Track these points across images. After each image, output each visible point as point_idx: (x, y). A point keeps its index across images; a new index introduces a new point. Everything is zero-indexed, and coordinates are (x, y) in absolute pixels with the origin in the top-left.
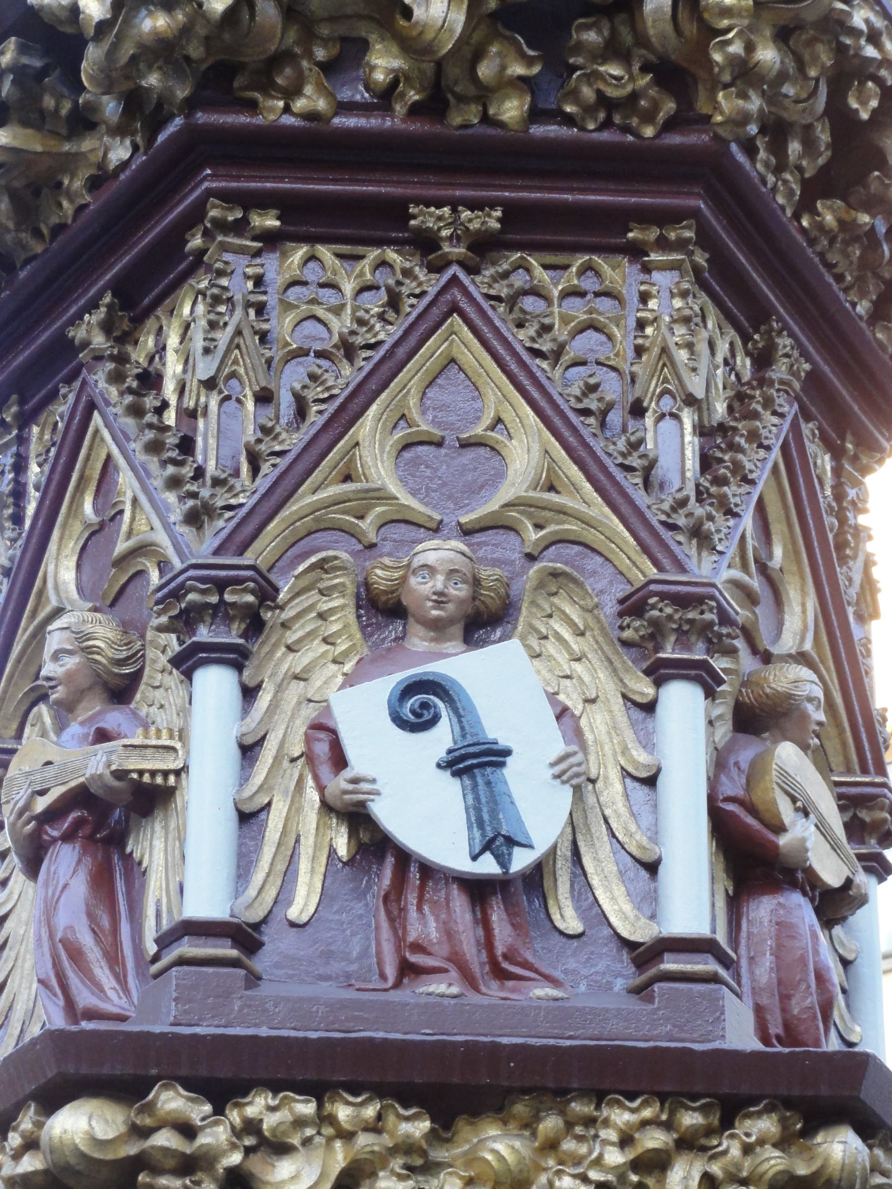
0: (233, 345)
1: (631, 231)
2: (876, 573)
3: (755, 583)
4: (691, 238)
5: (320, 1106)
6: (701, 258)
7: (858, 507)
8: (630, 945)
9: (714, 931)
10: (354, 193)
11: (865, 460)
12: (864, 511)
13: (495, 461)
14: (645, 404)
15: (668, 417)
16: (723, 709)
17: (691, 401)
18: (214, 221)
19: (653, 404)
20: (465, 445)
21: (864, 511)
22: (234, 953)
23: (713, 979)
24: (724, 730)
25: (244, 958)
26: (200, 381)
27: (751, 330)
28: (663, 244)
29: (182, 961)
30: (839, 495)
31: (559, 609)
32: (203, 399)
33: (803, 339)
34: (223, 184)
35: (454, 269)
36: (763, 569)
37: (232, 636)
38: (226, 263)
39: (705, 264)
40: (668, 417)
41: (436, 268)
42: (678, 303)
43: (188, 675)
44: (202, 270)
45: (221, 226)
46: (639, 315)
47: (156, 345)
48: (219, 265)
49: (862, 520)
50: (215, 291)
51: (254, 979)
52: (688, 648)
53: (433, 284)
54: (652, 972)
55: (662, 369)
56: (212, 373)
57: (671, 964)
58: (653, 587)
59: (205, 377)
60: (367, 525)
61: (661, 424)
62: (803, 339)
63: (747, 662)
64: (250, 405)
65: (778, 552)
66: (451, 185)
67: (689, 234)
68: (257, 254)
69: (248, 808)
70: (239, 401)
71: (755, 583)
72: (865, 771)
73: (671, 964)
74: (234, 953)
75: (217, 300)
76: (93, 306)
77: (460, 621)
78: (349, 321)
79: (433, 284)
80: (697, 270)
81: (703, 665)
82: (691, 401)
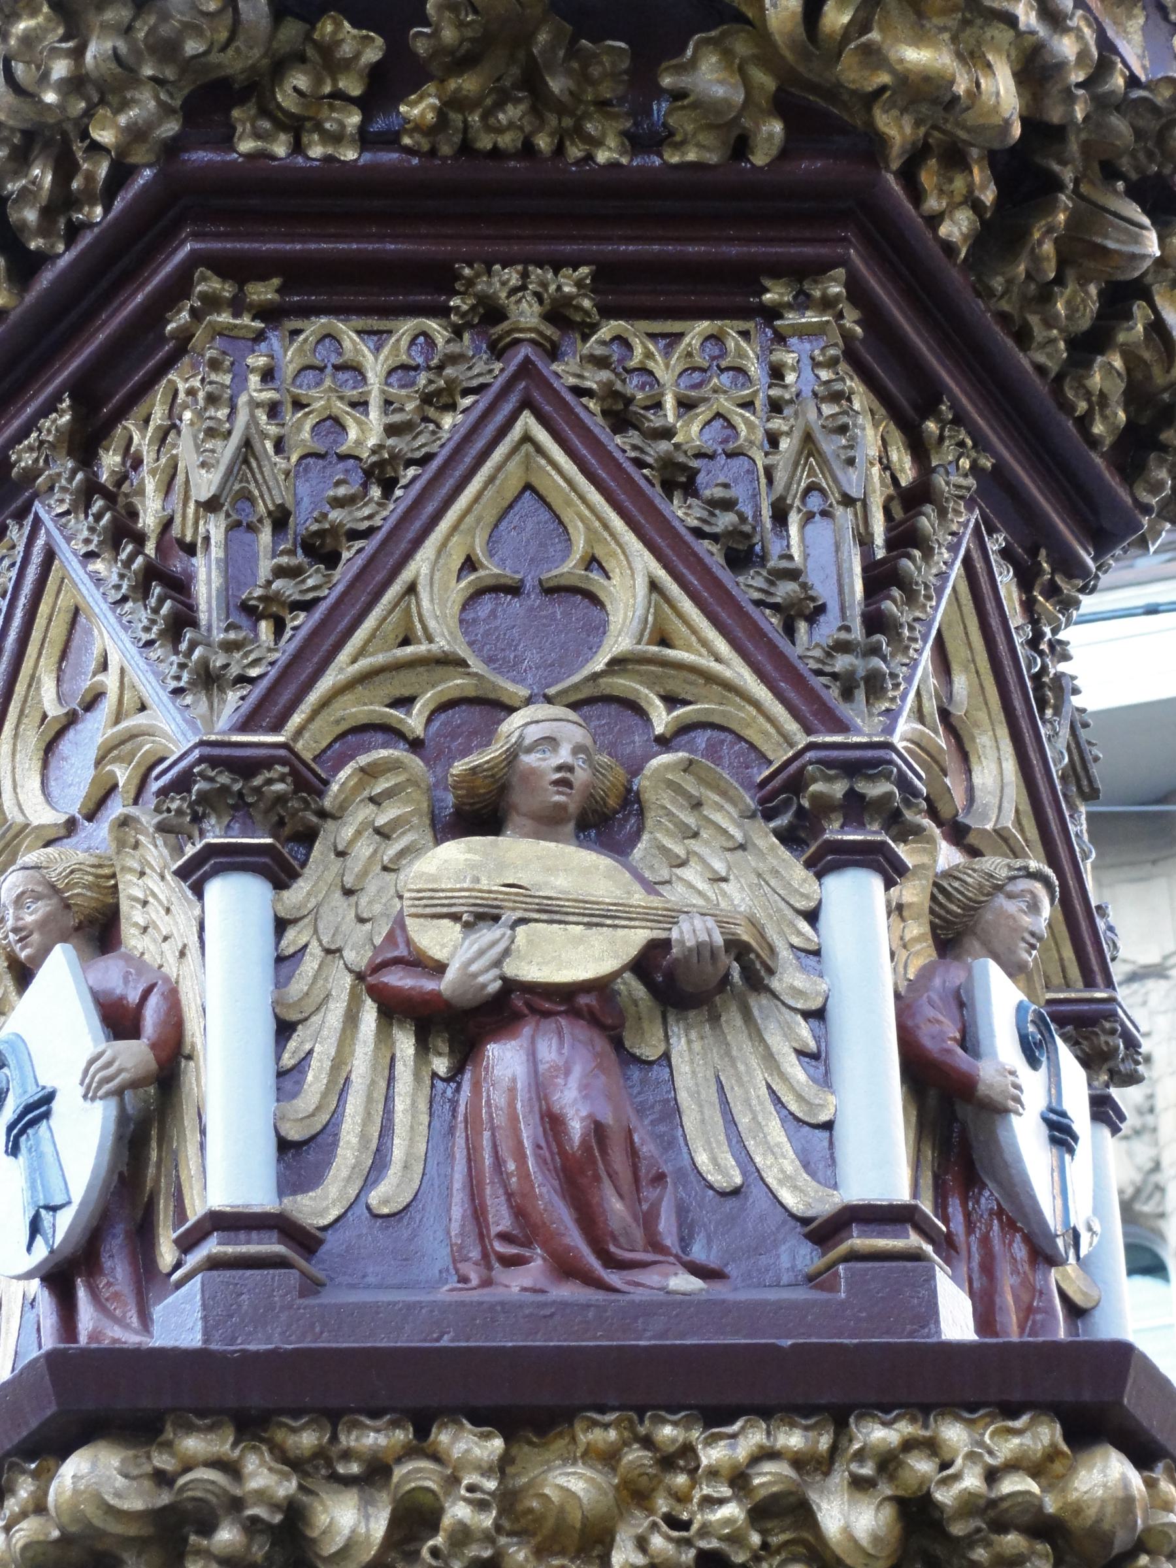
1: (767, 290)
4: (838, 295)
6: (851, 320)
8: (805, 1221)
9: (915, 1194)
13: (595, 611)
14: (789, 501)
15: (818, 517)
17: (848, 501)
18: (203, 297)
19: (797, 503)
20: (551, 591)
22: (279, 1249)
23: (916, 1256)
24: (924, 954)
28: (803, 302)
31: (696, 853)
32: (201, 529)
34: (217, 245)
35: (524, 351)
39: (858, 330)
40: (818, 517)
41: (498, 351)
43: (198, 891)
46: (772, 392)
52: (861, 825)
53: (498, 372)
54: (833, 1254)
55: (807, 459)
56: (213, 490)
57: (859, 1241)
59: (204, 495)
60: (415, 721)
61: (809, 527)
63: (948, 856)
65: (961, 682)
66: (507, 238)
67: (836, 289)
68: (260, 337)
73: (859, 1241)
74: (279, 1249)
76: (50, 408)
78: (202, 575)
79: (498, 372)
80: (847, 336)
82: (848, 501)
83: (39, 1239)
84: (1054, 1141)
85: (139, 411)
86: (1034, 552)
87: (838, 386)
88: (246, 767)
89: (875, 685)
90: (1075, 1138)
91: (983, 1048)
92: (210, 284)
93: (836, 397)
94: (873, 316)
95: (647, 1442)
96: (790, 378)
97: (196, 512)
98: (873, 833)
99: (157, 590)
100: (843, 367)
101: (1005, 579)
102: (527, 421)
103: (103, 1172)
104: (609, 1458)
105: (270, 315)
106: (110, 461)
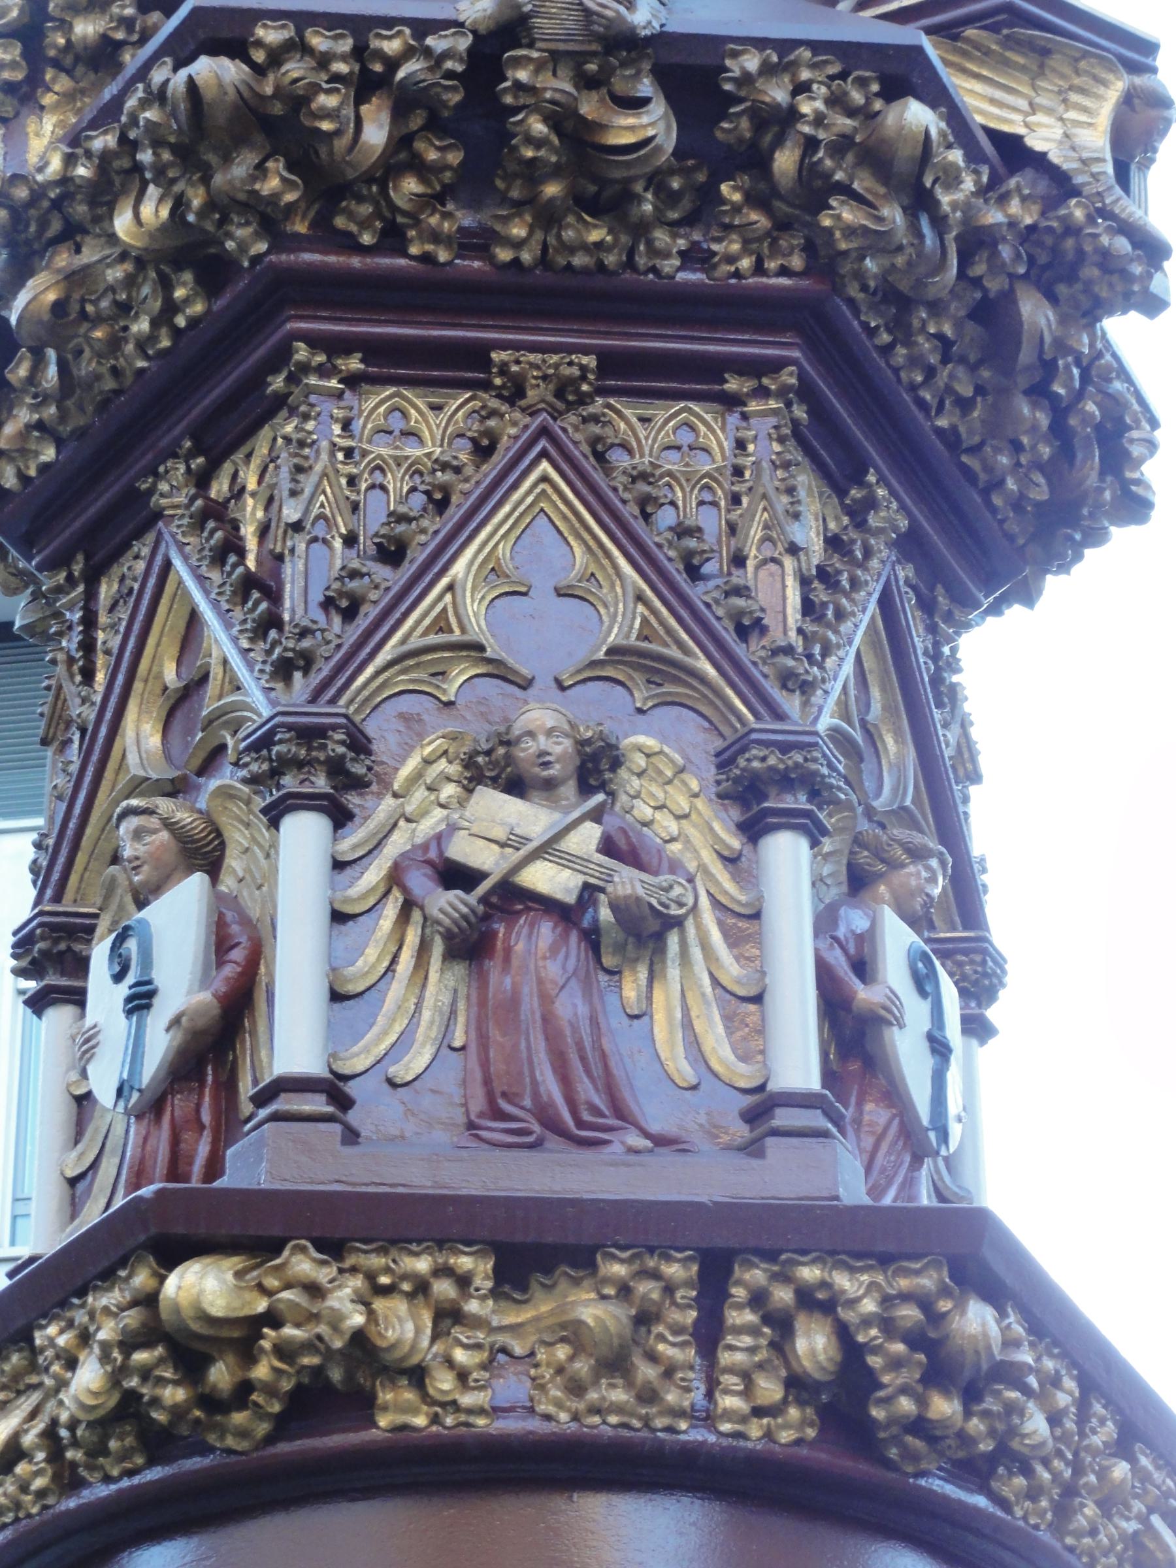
0: (318, 489)
2: (975, 733)
3: (858, 736)
5: (329, 359)
7: (953, 665)
10: (464, 338)
11: (957, 614)
12: (958, 671)
16: (835, 869)
19: (754, 552)
21: (958, 671)
22: (330, 1109)
23: (825, 1134)
24: (834, 893)
25: (339, 1114)
26: (287, 524)
27: (717, 387)
28: (762, 392)
29: (276, 1117)
30: (936, 656)
33: (908, 501)
36: (864, 723)
37: (321, 783)
38: (312, 405)
42: (777, 447)
43: (274, 823)
44: (284, 413)
45: (305, 368)
47: (231, 489)
48: (303, 408)
49: (955, 679)
50: (301, 435)
51: (351, 1136)
58: (754, 736)
62: (908, 501)
64: (338, 544)
69: (340, 858)
70: (325, 541)
71: (858, 736)
72: (966, 928)
73: (783, 1118)
74: (330, 1109)
75: (302, 444)
77: (569, 778)
80: (795, 423)
81: (807, 814)
83: (648, 1144)
84: (934, 1051)
85: (244, 450)
86: (932, 589)
87: (788, 457)
88: (310, 734)
89: (806, 688)
90: (950, 1051)
91: (875, 971)
92: (302, 352)
93: (786, 465)
94: (819, 410)
95: (656, 1275)
96: (751, 448)
97: (285, 532)
98: (799, 801)
99: (256, 595)
100: (791, 443)
101: (910, 601)
102: (545, 465)
103: (170, 1058)
104: (625, 1291)
105: (353, 381)
106: (219, 488)
